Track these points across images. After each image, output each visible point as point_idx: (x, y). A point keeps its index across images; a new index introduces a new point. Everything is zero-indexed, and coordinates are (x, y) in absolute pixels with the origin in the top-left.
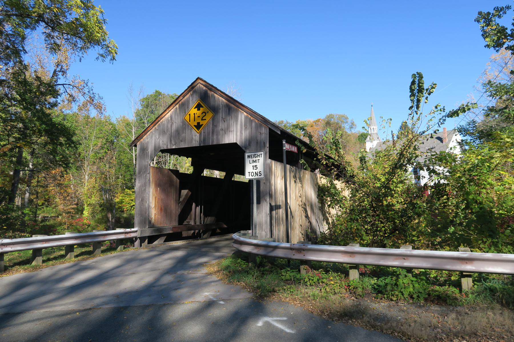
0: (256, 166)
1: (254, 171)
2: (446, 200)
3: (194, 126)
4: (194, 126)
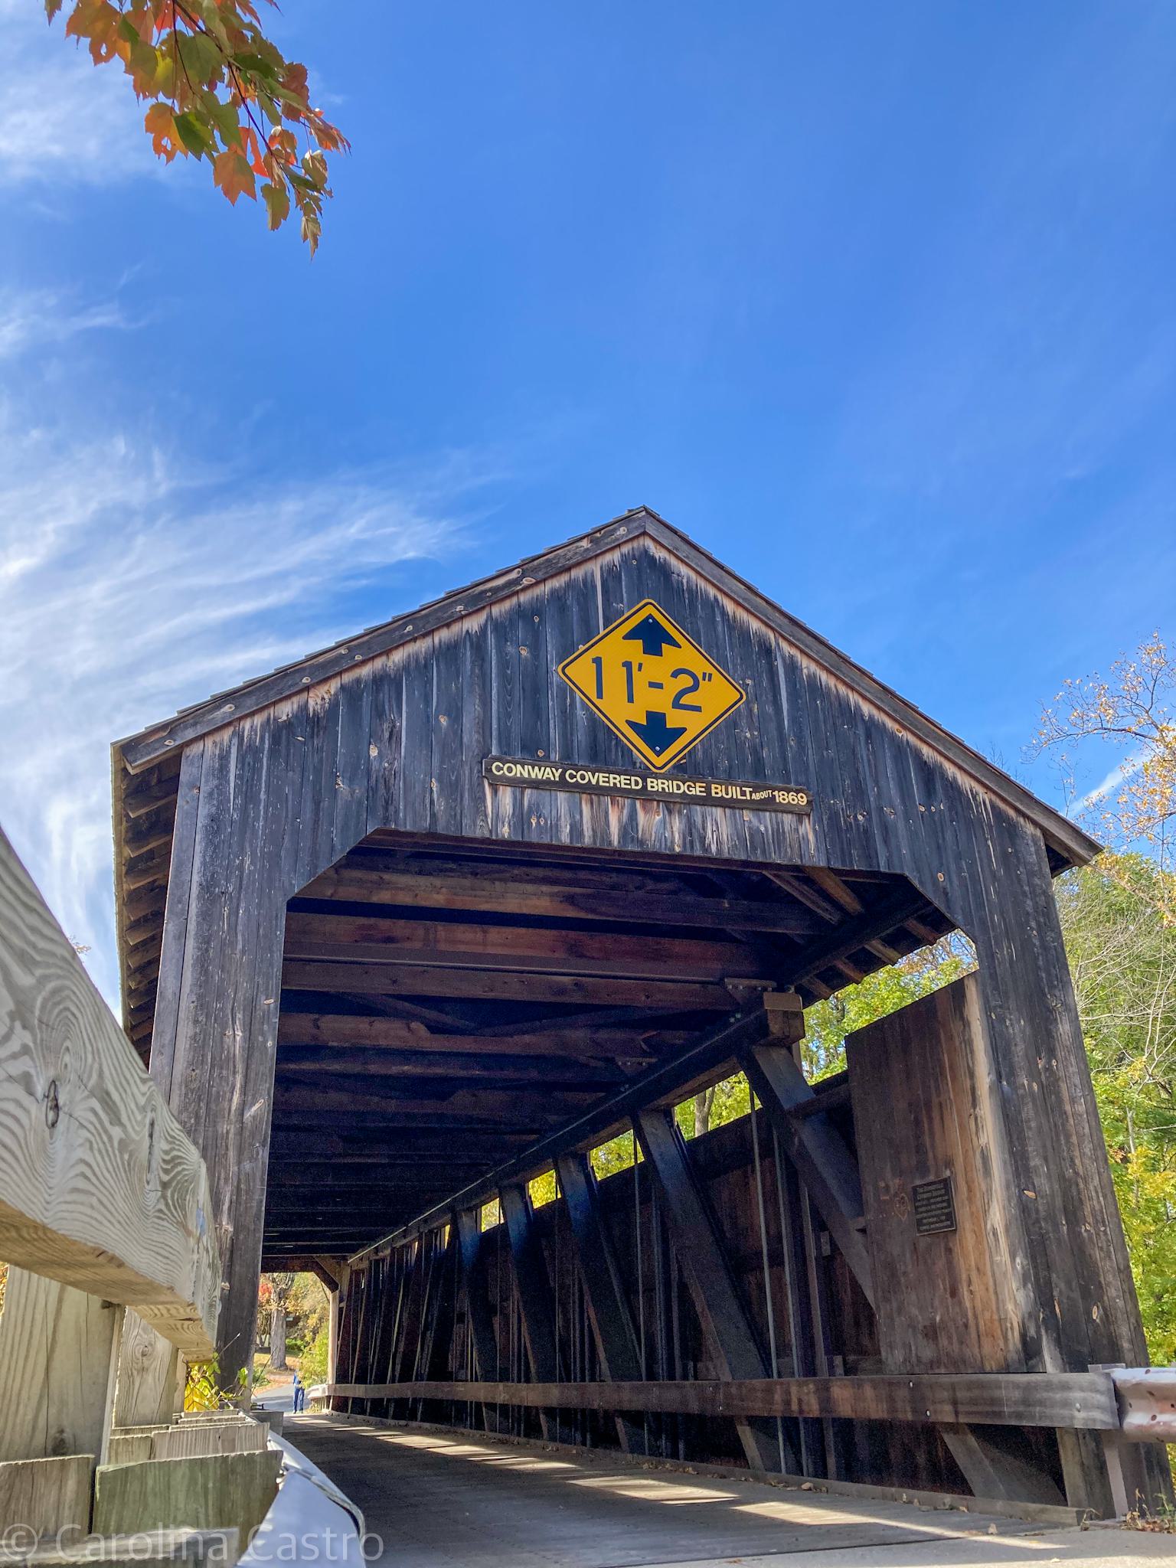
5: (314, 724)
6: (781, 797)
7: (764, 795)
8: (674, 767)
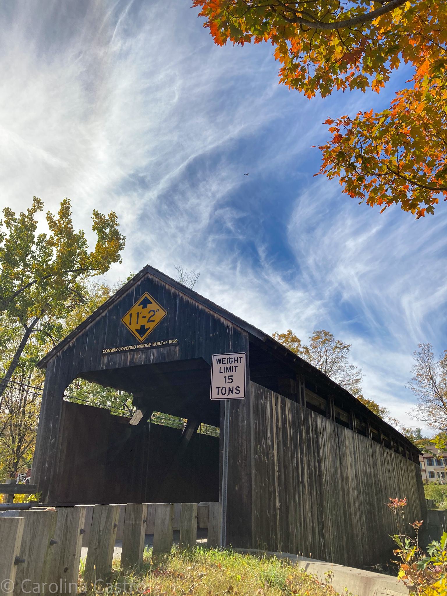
0: (230, 377)
1: (227, 386)
3: (151, 303)
4: (151, 303)
5: (70, 350)
6: (171, 342)
7: (166, 342)
8: (146, 340)
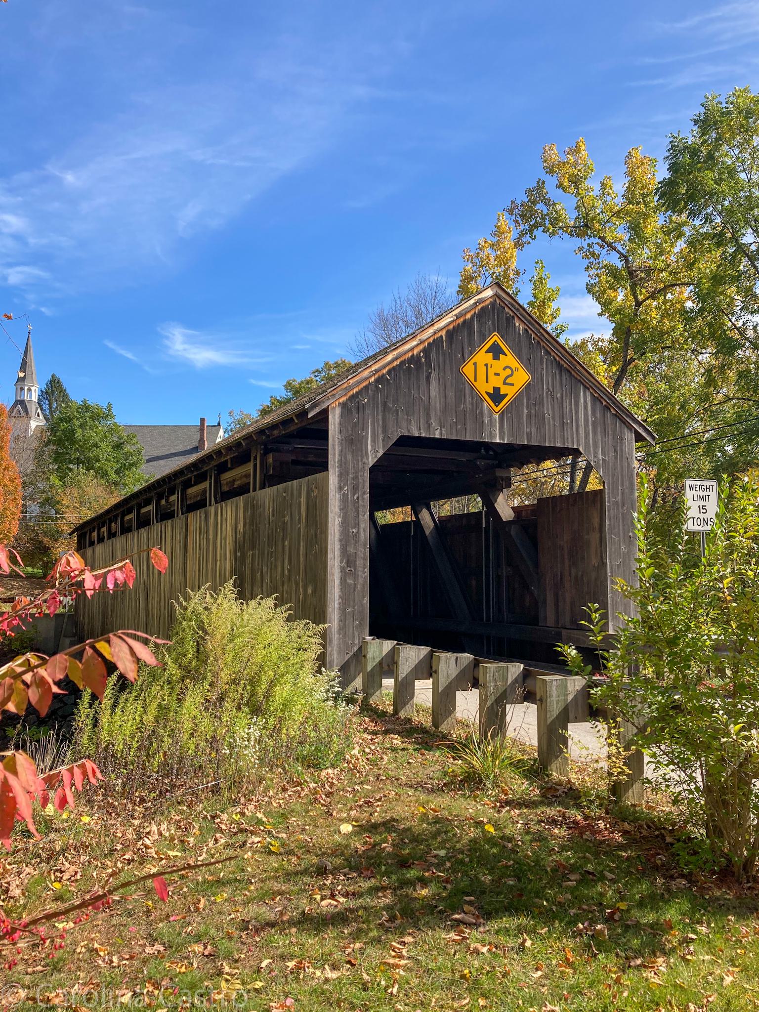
0: (704, 507)
1: (702, 516)
2: (603, 621)
3: (487, 393)
